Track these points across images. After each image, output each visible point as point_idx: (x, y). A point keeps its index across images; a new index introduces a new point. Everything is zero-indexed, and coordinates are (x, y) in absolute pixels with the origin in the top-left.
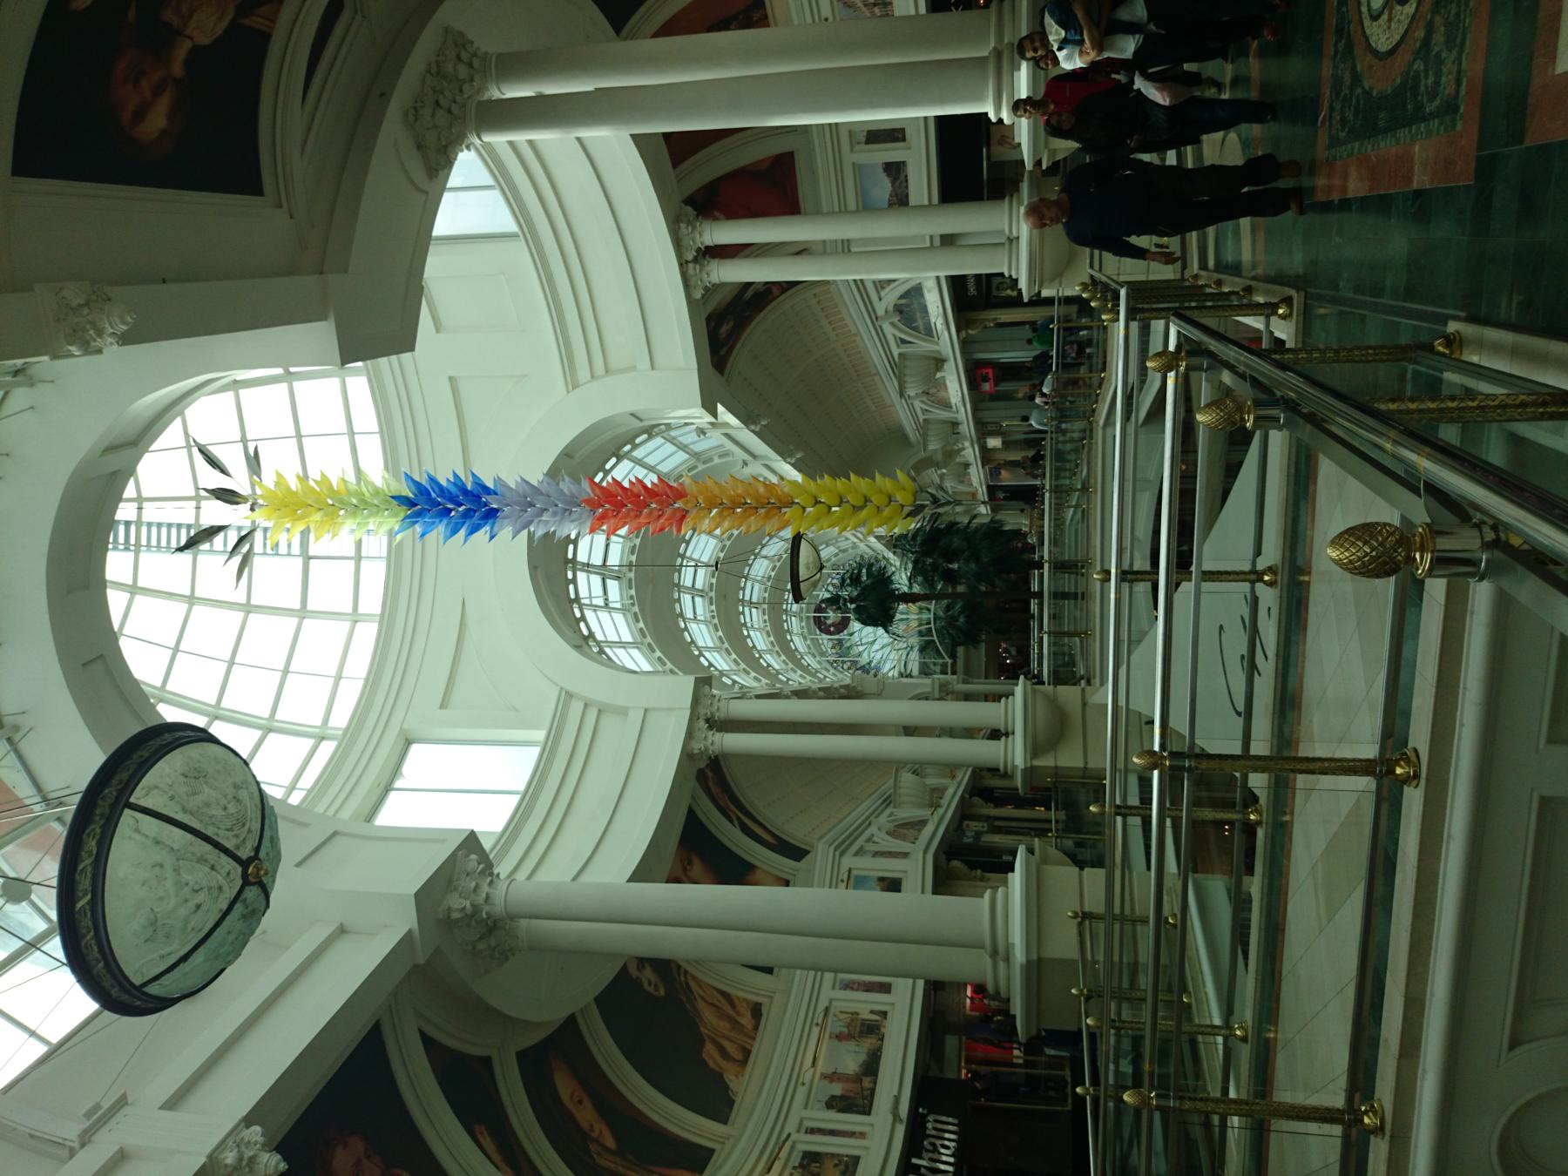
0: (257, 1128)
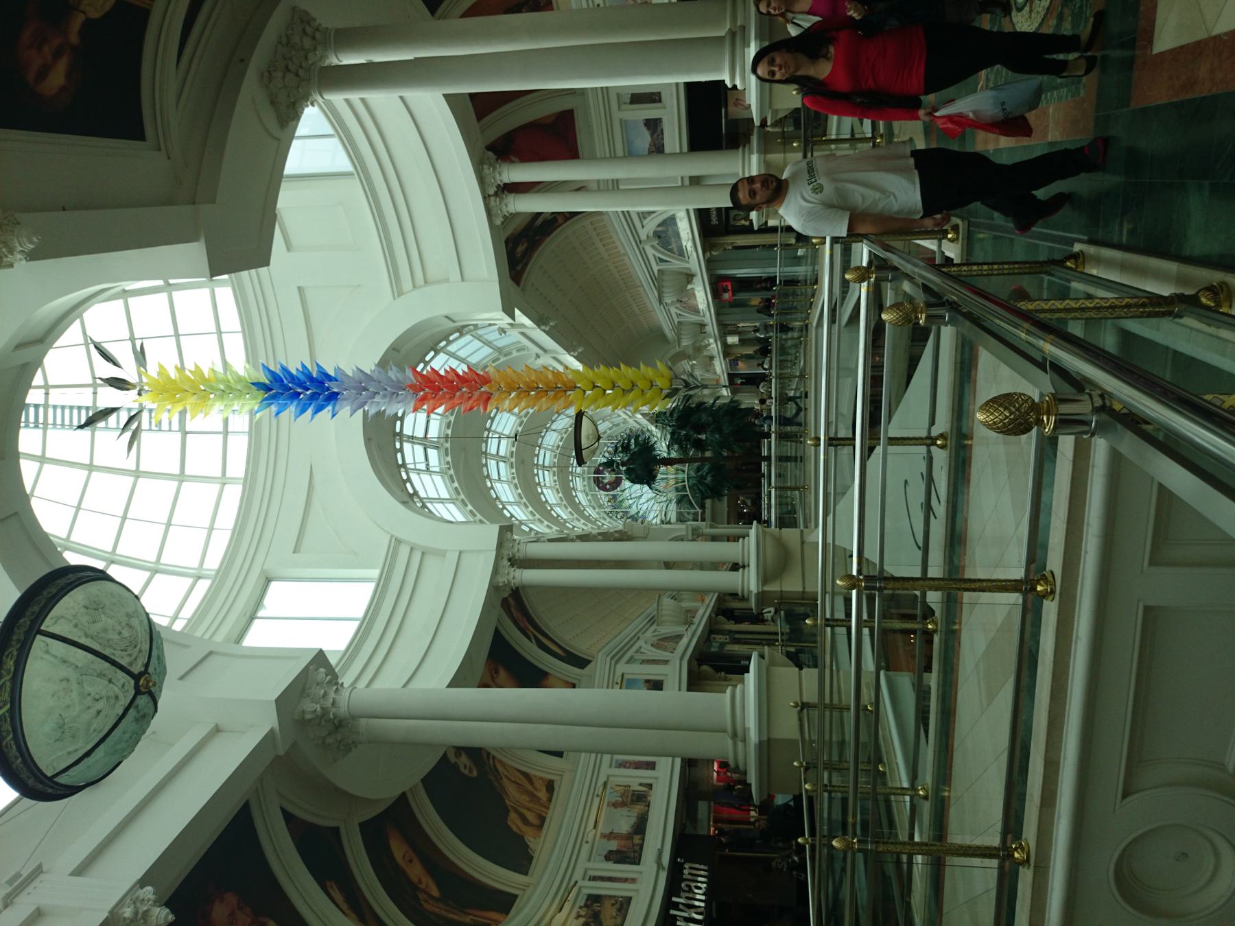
0: (149, 889)
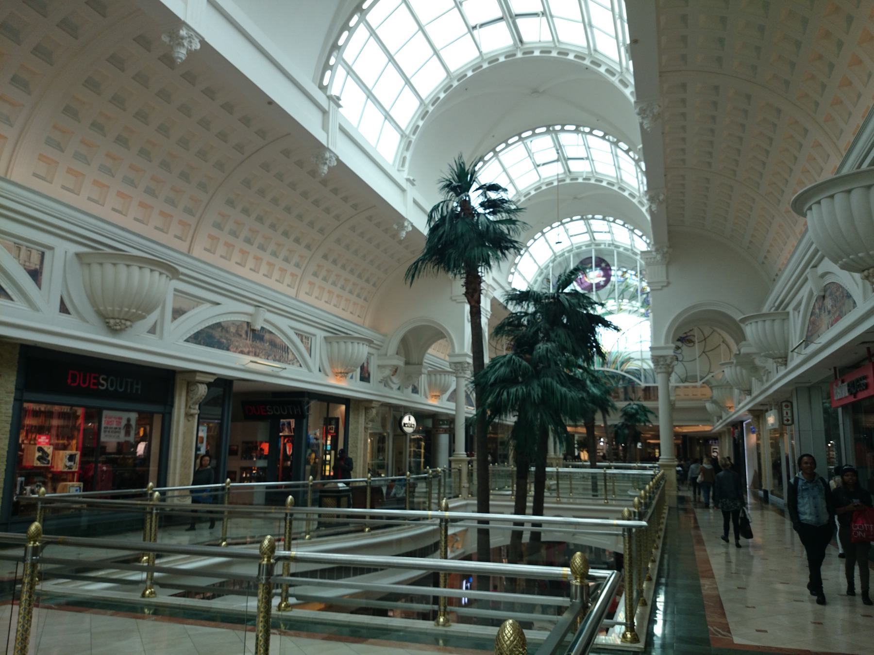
0: (198, 47)
